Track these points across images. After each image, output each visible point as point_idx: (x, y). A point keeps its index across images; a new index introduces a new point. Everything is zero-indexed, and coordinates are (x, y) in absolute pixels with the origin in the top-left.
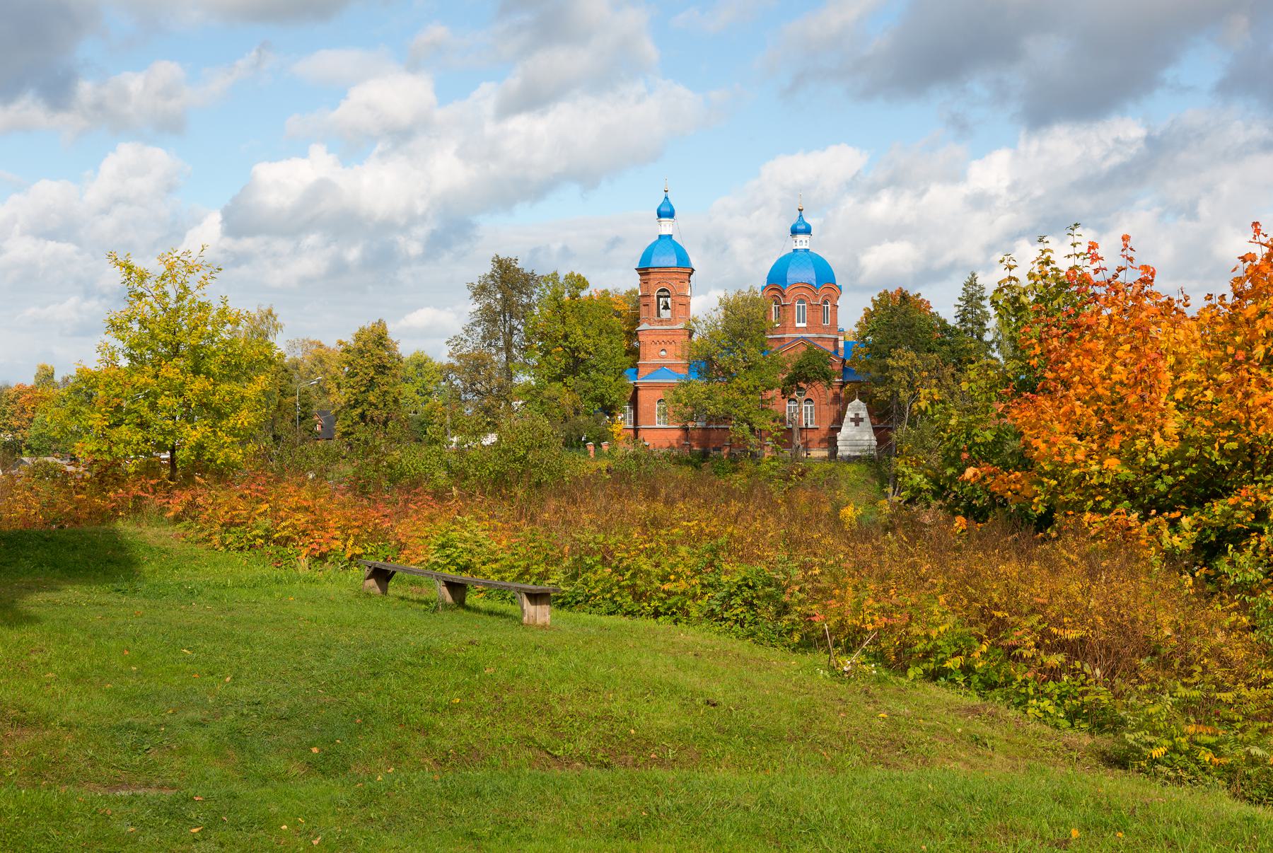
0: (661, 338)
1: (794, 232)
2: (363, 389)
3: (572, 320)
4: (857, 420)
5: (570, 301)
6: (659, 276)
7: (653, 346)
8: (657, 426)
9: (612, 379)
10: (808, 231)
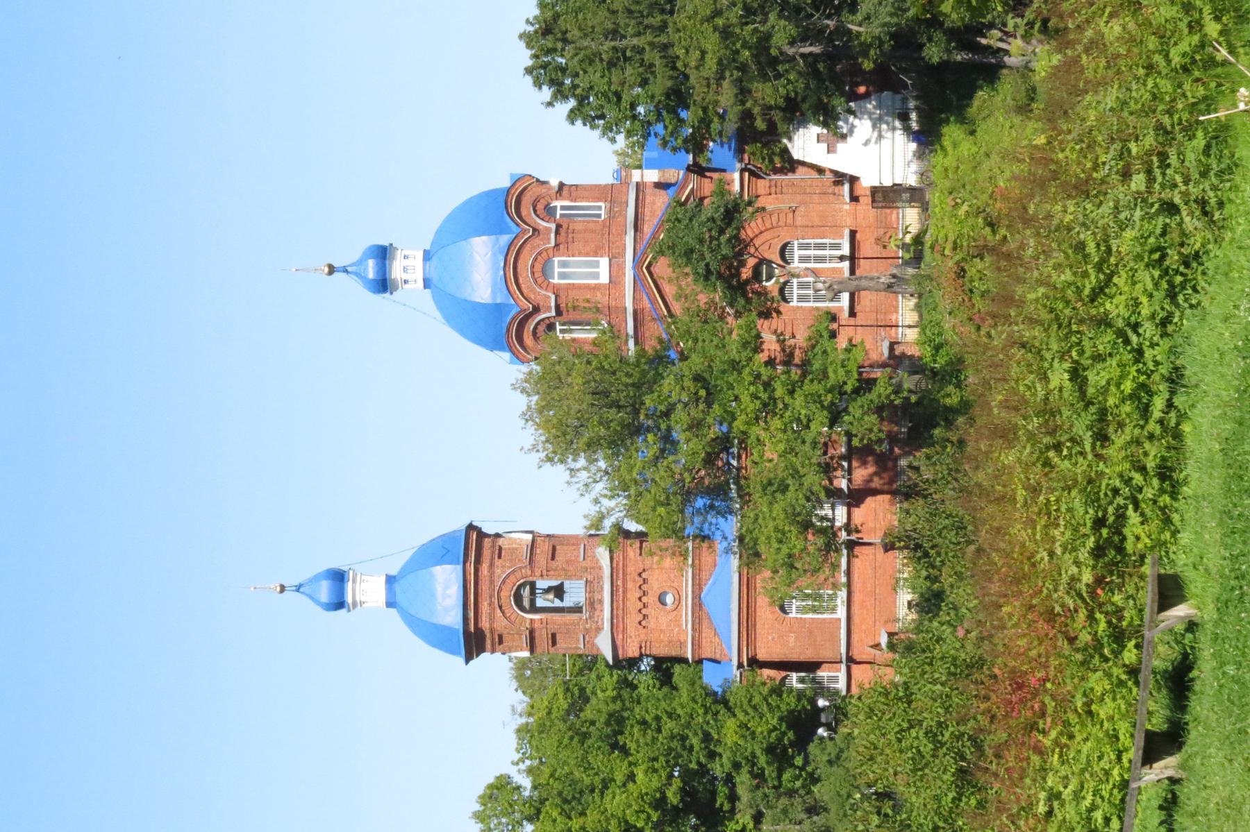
0: (633, 604)
1: (383, 285)
6: (485, 607)
9: (731, 724)
10: (383, 254)
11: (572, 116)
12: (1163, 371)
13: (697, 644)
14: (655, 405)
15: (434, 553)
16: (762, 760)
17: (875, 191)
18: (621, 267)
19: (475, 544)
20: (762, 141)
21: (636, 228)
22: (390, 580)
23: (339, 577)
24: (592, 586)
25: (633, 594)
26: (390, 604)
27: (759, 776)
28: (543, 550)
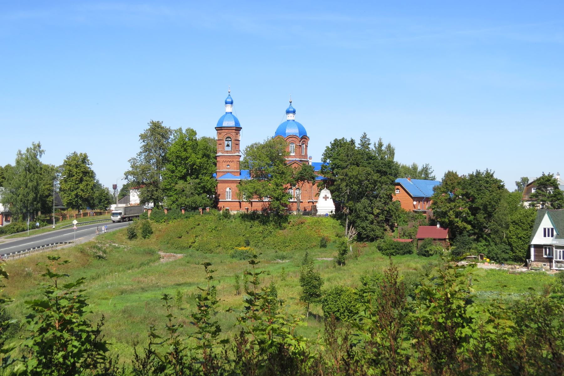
0: (227, 160)
1: (288, 112)
2: (77, 182)
3: (190, 151)
4: (326, 198)
5: (189, 142)
6: (227, 131)
7: (224, 163)
8: (227, 200)
9: (209, 178)
10: (294, 112)
11: (328, 147)
12: (402, 270)
13: (219, 172)
14: (273, 164)
15: (237, 122)
16: (202, 184)
17: (316, 206)
18: (293, 158)
19: (238, 129)
20: (328, 183)
21: (301, 161)
22: (231, 113)
23: (232, 103)
24: (227, 152)
25: (229, 160)
26: (226, 113)
27: (199, 184)
28: (237, 142)
